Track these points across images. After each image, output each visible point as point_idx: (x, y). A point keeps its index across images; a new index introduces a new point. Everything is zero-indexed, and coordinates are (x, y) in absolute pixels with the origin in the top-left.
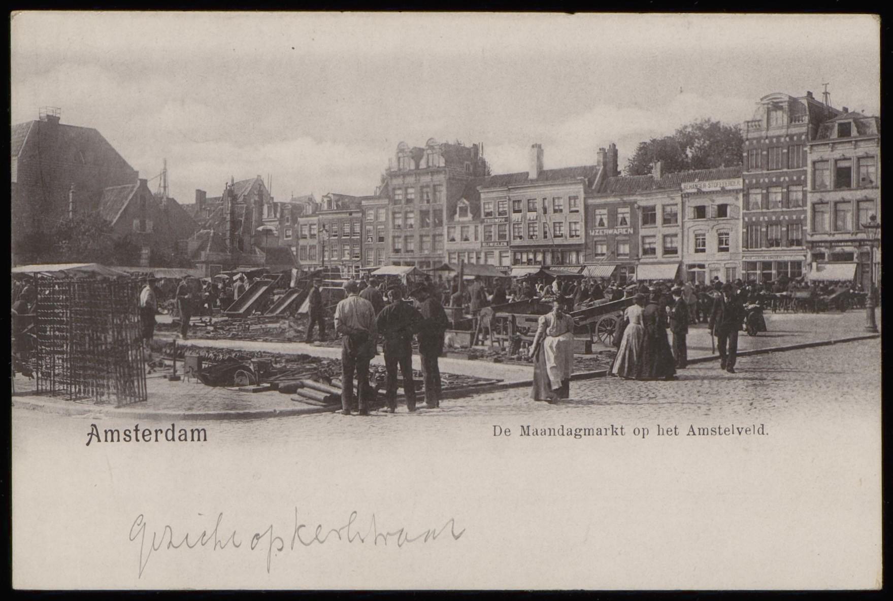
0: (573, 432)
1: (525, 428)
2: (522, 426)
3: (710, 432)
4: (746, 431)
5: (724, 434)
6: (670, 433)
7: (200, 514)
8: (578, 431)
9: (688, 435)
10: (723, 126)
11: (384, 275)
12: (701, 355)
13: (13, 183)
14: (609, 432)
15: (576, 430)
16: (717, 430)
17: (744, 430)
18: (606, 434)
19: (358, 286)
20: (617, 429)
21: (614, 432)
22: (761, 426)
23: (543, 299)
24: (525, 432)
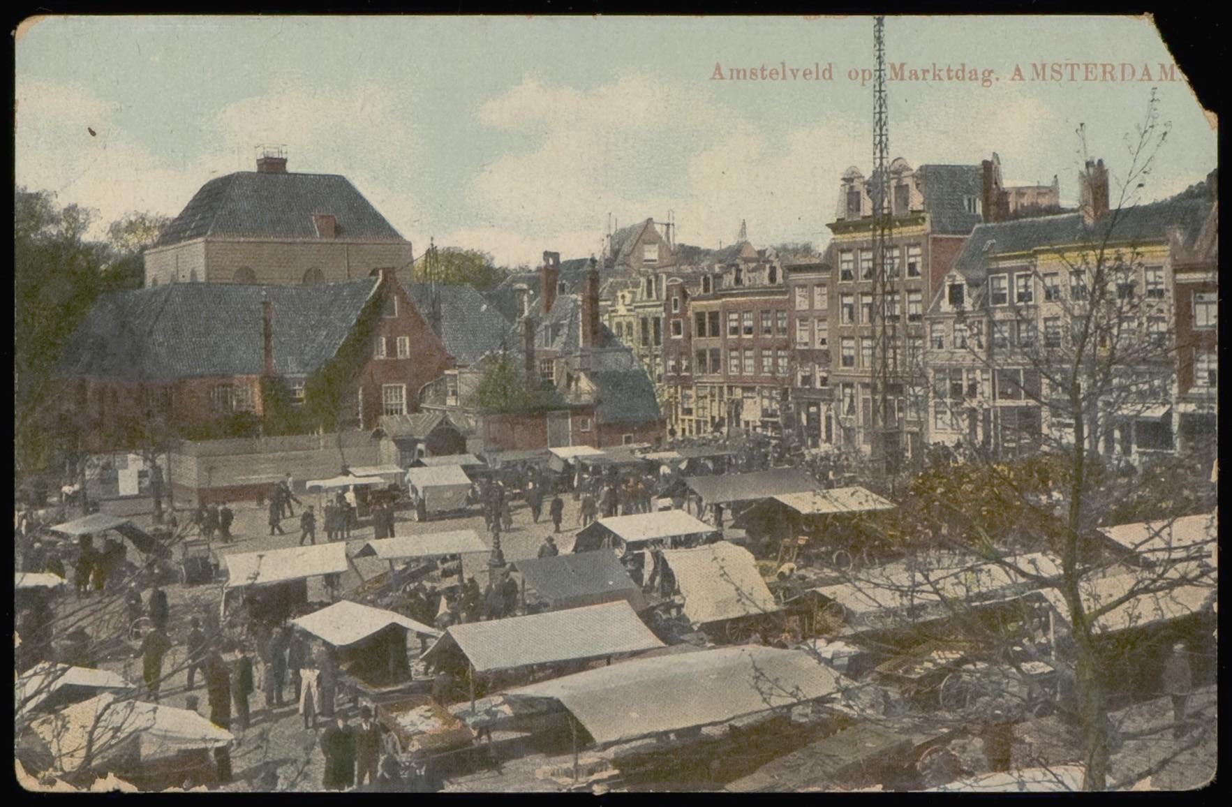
0: (980, 76)
1: (1039, 67)
2: (1034, 65)
3: (748, 74)
4: (805, 75)
5: (955, 79)
6: (775, 76)
7: (93, 133)
8: (986, 74)
9: (1013, 79)
10: (432, 253)
11: (610, 532)
12: (842, 775)
13: (1210, 350)
14: (930, 76)
15: (983, 74)
16: (759, 73)
17: (801, 73)
18: (1072, 79)
19: (387, 776)
20: (940, 70)
21: (936, 77)
22: (960, 68)
23: (1045, 381)
24: (1166, 76)
